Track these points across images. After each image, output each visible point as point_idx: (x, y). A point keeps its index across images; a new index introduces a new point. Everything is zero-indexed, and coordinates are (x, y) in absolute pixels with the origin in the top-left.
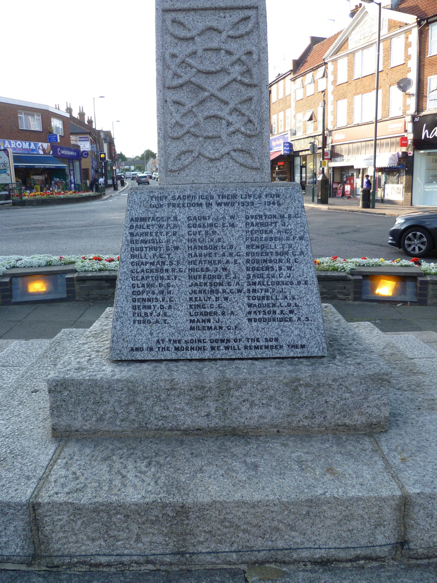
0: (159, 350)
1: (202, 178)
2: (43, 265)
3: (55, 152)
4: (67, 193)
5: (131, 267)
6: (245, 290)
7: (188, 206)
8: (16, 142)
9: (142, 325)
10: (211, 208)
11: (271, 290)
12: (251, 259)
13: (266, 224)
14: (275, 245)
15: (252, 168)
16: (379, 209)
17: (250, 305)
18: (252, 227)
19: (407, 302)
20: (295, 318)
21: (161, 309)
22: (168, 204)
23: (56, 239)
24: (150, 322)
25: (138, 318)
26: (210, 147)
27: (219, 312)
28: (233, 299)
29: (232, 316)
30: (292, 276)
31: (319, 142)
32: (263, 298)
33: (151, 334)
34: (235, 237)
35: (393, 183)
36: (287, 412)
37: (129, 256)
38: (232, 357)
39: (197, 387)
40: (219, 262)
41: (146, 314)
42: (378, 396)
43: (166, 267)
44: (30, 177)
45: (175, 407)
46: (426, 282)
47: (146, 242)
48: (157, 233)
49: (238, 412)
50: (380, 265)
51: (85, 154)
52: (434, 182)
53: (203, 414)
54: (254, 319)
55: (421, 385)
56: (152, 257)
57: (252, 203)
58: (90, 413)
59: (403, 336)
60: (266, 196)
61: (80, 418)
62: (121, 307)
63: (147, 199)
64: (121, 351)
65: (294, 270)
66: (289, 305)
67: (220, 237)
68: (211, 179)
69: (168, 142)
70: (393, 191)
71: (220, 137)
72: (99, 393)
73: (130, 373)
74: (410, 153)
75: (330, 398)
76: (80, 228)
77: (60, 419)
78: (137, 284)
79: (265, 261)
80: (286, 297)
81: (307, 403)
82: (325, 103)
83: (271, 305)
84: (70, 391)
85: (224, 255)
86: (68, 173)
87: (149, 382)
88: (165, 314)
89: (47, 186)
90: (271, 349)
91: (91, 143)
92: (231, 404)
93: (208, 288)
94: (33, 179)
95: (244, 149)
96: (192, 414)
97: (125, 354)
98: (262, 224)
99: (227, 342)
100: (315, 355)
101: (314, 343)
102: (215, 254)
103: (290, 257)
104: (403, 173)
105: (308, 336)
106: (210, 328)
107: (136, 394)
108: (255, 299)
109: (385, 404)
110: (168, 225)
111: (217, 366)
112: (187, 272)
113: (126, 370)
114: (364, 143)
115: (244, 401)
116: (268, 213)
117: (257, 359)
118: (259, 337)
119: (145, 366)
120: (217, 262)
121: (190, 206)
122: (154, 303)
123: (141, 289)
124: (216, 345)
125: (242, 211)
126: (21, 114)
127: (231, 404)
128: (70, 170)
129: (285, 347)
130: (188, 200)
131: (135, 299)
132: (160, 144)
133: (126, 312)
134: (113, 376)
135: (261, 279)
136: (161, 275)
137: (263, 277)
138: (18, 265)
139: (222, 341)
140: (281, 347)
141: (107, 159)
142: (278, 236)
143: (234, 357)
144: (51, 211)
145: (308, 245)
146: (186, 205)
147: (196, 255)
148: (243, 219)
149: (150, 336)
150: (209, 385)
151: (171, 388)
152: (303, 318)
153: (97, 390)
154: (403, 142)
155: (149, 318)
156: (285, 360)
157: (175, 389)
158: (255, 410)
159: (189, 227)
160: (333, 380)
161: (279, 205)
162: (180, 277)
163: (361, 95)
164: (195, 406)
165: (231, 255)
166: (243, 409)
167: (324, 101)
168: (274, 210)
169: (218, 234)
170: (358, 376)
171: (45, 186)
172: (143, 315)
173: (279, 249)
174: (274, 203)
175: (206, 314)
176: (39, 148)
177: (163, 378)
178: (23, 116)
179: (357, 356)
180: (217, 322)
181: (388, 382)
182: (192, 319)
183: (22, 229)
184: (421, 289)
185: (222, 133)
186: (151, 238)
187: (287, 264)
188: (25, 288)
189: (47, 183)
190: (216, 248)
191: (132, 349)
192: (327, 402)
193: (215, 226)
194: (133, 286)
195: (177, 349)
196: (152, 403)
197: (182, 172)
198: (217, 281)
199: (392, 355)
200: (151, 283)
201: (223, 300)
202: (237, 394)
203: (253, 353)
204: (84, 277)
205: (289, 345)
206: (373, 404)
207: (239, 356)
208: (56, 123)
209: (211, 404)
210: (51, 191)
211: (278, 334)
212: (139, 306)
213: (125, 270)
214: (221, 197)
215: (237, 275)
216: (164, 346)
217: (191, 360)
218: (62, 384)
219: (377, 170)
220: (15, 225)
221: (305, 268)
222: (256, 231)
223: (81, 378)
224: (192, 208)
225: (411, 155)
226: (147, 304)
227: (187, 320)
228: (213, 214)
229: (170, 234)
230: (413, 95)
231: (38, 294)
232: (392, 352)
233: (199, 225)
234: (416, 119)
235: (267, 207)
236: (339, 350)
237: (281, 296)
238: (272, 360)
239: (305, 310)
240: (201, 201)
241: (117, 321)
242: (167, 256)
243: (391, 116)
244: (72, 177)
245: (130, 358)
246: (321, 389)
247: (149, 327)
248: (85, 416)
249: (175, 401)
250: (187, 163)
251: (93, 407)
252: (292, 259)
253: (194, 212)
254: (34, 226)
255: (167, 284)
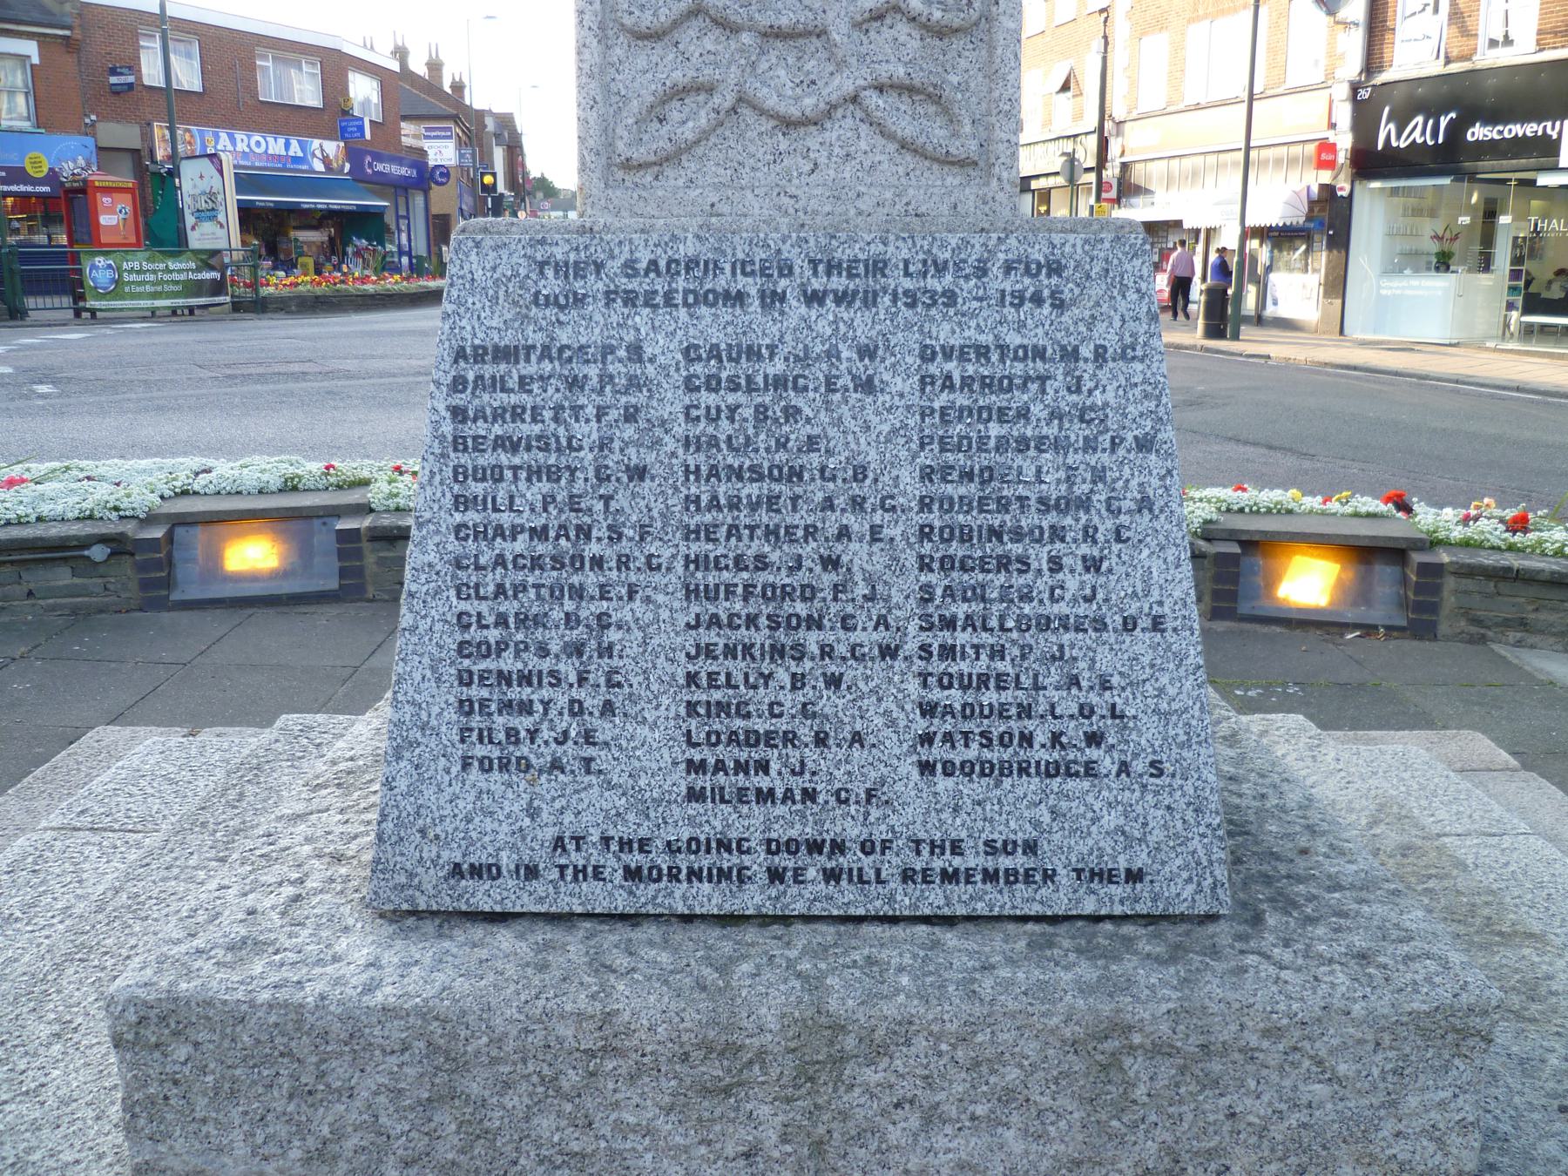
0: (562, 876)
1: (749, 195)
2: (274, 488)
3: (357, 168)
4: (385, 278)
5: (453, 545)
6: (911, 647)
7: (686, 304)
8: (249, 137)
9: (496, 775)
10: (782, 313)
11: (1016, 652)
12: (937, 524)
13: (1005, 385)
14: (1039, 470)
15: (948, 161)
16: (1251, 343)
17: (928, 710)
18: (944, 396)
19: (1376, 627)
20: (1108, 764)
21: (573, 714)
22: (607, 293)
23: (335, 408)
24: (529, 766)
25: (480, 751)
26: (782, 73)
27: (805, 732)
28: (861, 684)
29: (856, 752)
30: (1100, 596)
31: (1087, 153)
32: (983, 680)
33: (533, 813)
34: (878, 434)
35: (1291, 270)
36: (1072, 1151)
37: (448, 501)
38: (852, 911)
39: (708, 1047)
40: (811, 532)
41: (512, 733)
42: (1442, 1094)
43: (593, 549)
44: (286, 234)
45: (618, 1123)
46: (1436, 570)
47: (515, 448)
48: (558, 409)
49: (873, 1147)
50: (1290, 512)
51: (442, 174)
52: (1407, 272)
53: (730, 1151)
54: (945, 764)
55: (1543, 991)
56: (539, 505)
57: (951, 297)
58: (282, 1130)
59: (1390, 748)
60: (1008, 268)
61: (241, 1150)
62: (413, 703)
63: (523, 272)
64: (411, 875)
65: (1110, 571)
66: (1086, 711)
67: (817, 431)
68: (786, 200)
69: (618, 51)
70: (1295, 289)
71: (822, 33)
72: (314, 1059)
73: (440, 978)
74: (1342, 189)
75: (1249, 1102)
76: (411, 379)
77: (162, 1148)
78: (479, 614)
79: (996, 533)
80: (1075, 681)
81: (1153, 1118)
82: (1106, 44)
83: (1013, 711)
84: (196, 1044)
85: (828, 504)
86: (393, 227)
87: (511, 1021)
88: (589, 737)
89: (335, 259)
90: (1007, 882)
91: (460, 144)
92: (844, 1116)
93: (760, 637)
94: (296, 240)
95: (917, 82)
96: (686, 1149)
97: (428, 887)
98: (987, 384)
99: (832, 852)
100: (1182, 908)
101: (1179, 862)
102: (795, 499)
103: (1096, 520)
104: (1321, 242)
105: (1157, 835)
106: (765, 796)
107: (459, 1065)
108: (950, 686)
109: (1463, 1126)
110: (606, 379)
111: (793, 954)
112: (680, 570)
113: (427, 958)
114: (1212, 159)
115: (897, 1106)
116: (1013, 339)
117: (949, 921)
118: (963, 835)
119: (505, 938)
120: (800, 533)
121: (696, 302)
122: (546, 693)
123: (493, 635)
124: (791, 864)
125: (909, 326)
126: (265, 58)
127: (844, 1116)
128: (398, 217)
129: (1064, 878)
130: (690, 279)
131: (471, 673)
132: (587, 56)
133: (434, 722)
134: (369, 989)
135: (977, 607)
136: (575, 579)
137: (983, 599)
138: (196, 487)
139: (815, 847)
140: (1049, 876)
141: (501, 188)
142: (1052, 431)
143: (861, 911)
144: (337, 329)
145: (1169, 472)
146: (679, 299)
147: (714, 504)
148: (910, 360)
149: (527, 821)
150: (756, 1042)
151: (603, 1049)
152: (1139, 766)
153: (302, 1046)
154: (1324, 157)
155: (524, 750)
156: (1062, 929)
157: (616, 1052)
158: (940, 1142)
159: (690, 386)
160: (1266, 1033)
161: (1060, 305)
162: (649, 592)
163: (1207, 22)
164: (700, 1120)
165: (857, 504)
166: (895, 1135)
167: (1105, 37)
168: (1039, 327)
169: (808, 420)
170: (1371, 1019)
171: (329, 260)
172: (502, 736)
173: (1053, 487)
174: (1037, 300)
175: (752, 739)
176: (314, 155)
177: (568, 1007)
178: (270, 64)
179: (1345, 915)
180: (793, 772)
181: (1483, 1038)
182: (697, 758)
183: (246, 378)
184: (1419, 589)
185: (831, 15)
186: (537, 428)
187: (1085, 549)
188: (216, 558)
189: (335, 250)
190: (796, 474)
191: (457, 871)
192: (1233, 1115)
193: (795, 388)
194: (462, 622)
195: (632, 874)
196: (527, 1101)
197: (669, 172)
198: (801, 608)
199: (1406, 850)
200: (535, 610)
201: (821, 684)
202: (871, 1076)
203: (934, 899)
204: (391, 528)
205: (1079, 872)
206: (1417, 1124)
207: (879, 907)
208: (363, 91)
209: (764, 1111)
210: (344, 274)
211: (1036, 824)
212: (484, 703)
213: (432, 557)
214: (821, 268)
215: (879, 588)
216: (581, 863)
217: (688, 919)
218: (163, 1019)
219: (1248, 233)
220: (228, 366)
221: (1156, 565)
222: (961, 410)
223: (240, 995)
224: (704, 310)
225: (1345, 194)
226: (516, 693)
227: (675, 764)
228: (788, 338)
229: (613, 414)
230: (1357, 25)
231: (253, 577)
232: (1405, 839)
233: (730, 379)
234: (1362, 92)
235: (1009, 311)
236: (1267, 879)
237: (1054, 676)
238: (1011, 927)
239: (1148, 733)
240: (742, 282)
241: (399, 758)
242: (599, 506)
243: (1292, 82)
244: (404, 237)
245: (447, 903)
246: (1216, 1067)
247: (523, 785)
248: (259, 1140)
249: (618, 1096)
250: (690, 136)
251: (291, 1108)
252: (1105, 526)
253: (713, 327)
254: (282, 368)
255: (599, 617)
